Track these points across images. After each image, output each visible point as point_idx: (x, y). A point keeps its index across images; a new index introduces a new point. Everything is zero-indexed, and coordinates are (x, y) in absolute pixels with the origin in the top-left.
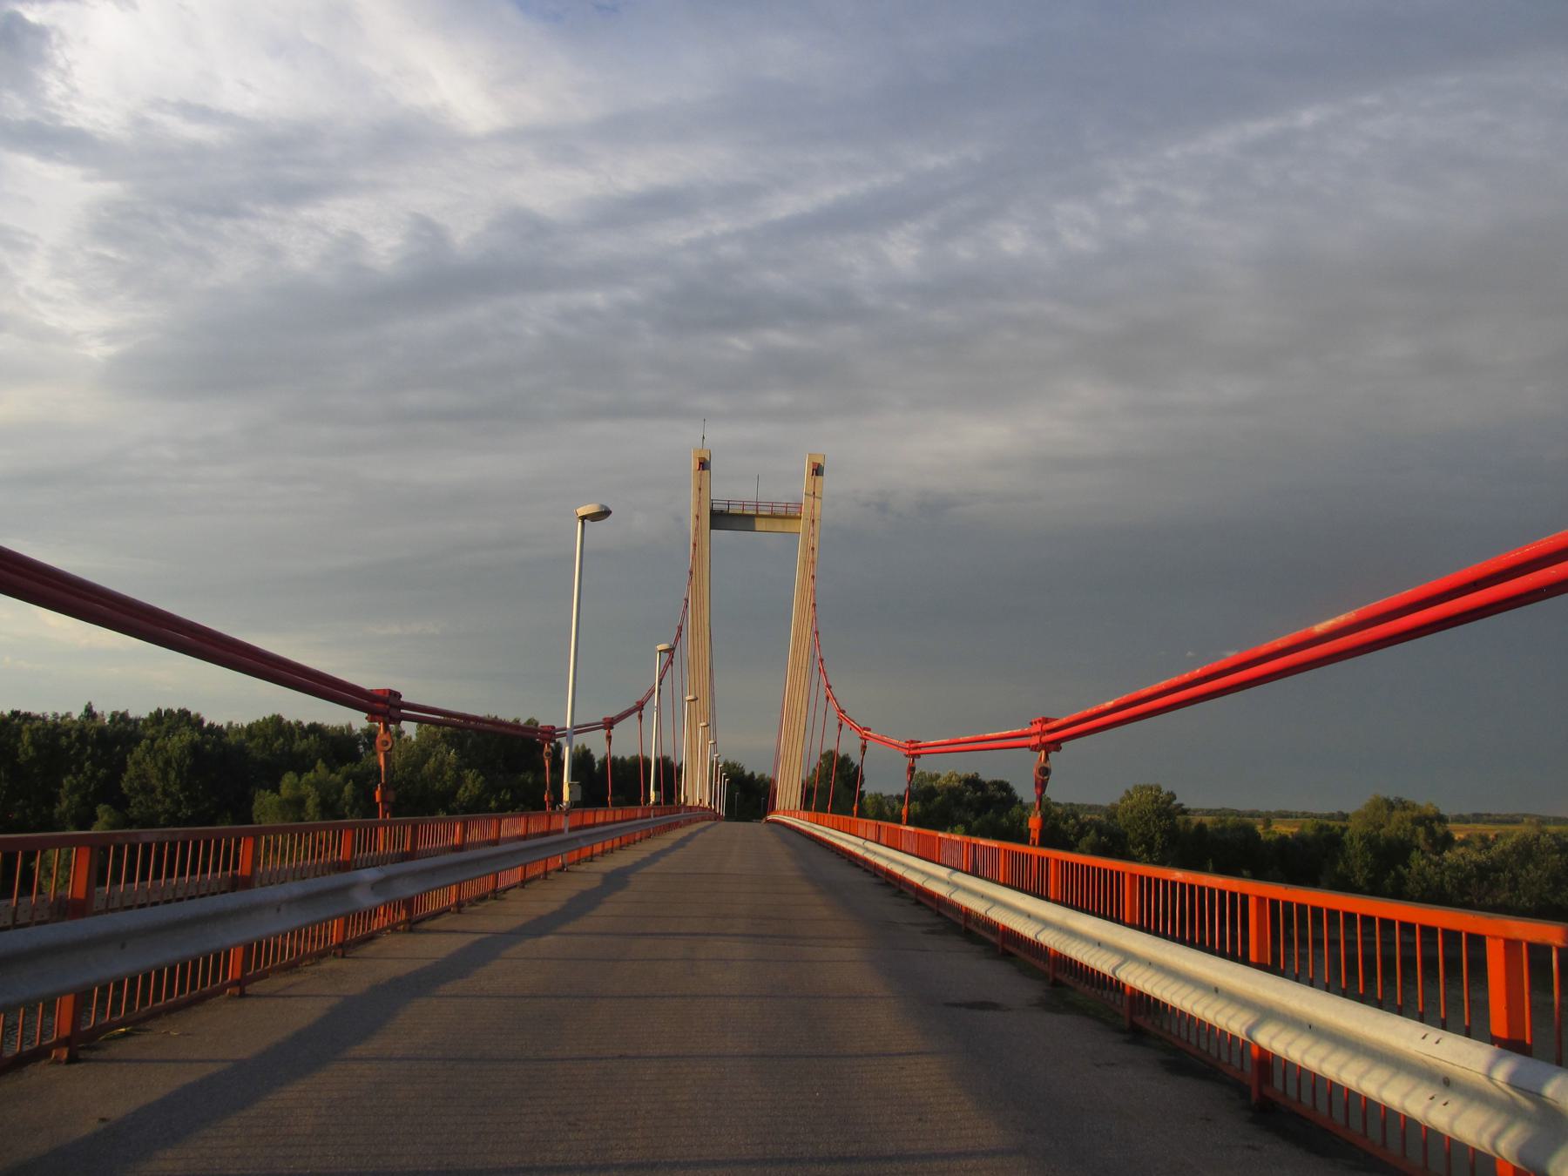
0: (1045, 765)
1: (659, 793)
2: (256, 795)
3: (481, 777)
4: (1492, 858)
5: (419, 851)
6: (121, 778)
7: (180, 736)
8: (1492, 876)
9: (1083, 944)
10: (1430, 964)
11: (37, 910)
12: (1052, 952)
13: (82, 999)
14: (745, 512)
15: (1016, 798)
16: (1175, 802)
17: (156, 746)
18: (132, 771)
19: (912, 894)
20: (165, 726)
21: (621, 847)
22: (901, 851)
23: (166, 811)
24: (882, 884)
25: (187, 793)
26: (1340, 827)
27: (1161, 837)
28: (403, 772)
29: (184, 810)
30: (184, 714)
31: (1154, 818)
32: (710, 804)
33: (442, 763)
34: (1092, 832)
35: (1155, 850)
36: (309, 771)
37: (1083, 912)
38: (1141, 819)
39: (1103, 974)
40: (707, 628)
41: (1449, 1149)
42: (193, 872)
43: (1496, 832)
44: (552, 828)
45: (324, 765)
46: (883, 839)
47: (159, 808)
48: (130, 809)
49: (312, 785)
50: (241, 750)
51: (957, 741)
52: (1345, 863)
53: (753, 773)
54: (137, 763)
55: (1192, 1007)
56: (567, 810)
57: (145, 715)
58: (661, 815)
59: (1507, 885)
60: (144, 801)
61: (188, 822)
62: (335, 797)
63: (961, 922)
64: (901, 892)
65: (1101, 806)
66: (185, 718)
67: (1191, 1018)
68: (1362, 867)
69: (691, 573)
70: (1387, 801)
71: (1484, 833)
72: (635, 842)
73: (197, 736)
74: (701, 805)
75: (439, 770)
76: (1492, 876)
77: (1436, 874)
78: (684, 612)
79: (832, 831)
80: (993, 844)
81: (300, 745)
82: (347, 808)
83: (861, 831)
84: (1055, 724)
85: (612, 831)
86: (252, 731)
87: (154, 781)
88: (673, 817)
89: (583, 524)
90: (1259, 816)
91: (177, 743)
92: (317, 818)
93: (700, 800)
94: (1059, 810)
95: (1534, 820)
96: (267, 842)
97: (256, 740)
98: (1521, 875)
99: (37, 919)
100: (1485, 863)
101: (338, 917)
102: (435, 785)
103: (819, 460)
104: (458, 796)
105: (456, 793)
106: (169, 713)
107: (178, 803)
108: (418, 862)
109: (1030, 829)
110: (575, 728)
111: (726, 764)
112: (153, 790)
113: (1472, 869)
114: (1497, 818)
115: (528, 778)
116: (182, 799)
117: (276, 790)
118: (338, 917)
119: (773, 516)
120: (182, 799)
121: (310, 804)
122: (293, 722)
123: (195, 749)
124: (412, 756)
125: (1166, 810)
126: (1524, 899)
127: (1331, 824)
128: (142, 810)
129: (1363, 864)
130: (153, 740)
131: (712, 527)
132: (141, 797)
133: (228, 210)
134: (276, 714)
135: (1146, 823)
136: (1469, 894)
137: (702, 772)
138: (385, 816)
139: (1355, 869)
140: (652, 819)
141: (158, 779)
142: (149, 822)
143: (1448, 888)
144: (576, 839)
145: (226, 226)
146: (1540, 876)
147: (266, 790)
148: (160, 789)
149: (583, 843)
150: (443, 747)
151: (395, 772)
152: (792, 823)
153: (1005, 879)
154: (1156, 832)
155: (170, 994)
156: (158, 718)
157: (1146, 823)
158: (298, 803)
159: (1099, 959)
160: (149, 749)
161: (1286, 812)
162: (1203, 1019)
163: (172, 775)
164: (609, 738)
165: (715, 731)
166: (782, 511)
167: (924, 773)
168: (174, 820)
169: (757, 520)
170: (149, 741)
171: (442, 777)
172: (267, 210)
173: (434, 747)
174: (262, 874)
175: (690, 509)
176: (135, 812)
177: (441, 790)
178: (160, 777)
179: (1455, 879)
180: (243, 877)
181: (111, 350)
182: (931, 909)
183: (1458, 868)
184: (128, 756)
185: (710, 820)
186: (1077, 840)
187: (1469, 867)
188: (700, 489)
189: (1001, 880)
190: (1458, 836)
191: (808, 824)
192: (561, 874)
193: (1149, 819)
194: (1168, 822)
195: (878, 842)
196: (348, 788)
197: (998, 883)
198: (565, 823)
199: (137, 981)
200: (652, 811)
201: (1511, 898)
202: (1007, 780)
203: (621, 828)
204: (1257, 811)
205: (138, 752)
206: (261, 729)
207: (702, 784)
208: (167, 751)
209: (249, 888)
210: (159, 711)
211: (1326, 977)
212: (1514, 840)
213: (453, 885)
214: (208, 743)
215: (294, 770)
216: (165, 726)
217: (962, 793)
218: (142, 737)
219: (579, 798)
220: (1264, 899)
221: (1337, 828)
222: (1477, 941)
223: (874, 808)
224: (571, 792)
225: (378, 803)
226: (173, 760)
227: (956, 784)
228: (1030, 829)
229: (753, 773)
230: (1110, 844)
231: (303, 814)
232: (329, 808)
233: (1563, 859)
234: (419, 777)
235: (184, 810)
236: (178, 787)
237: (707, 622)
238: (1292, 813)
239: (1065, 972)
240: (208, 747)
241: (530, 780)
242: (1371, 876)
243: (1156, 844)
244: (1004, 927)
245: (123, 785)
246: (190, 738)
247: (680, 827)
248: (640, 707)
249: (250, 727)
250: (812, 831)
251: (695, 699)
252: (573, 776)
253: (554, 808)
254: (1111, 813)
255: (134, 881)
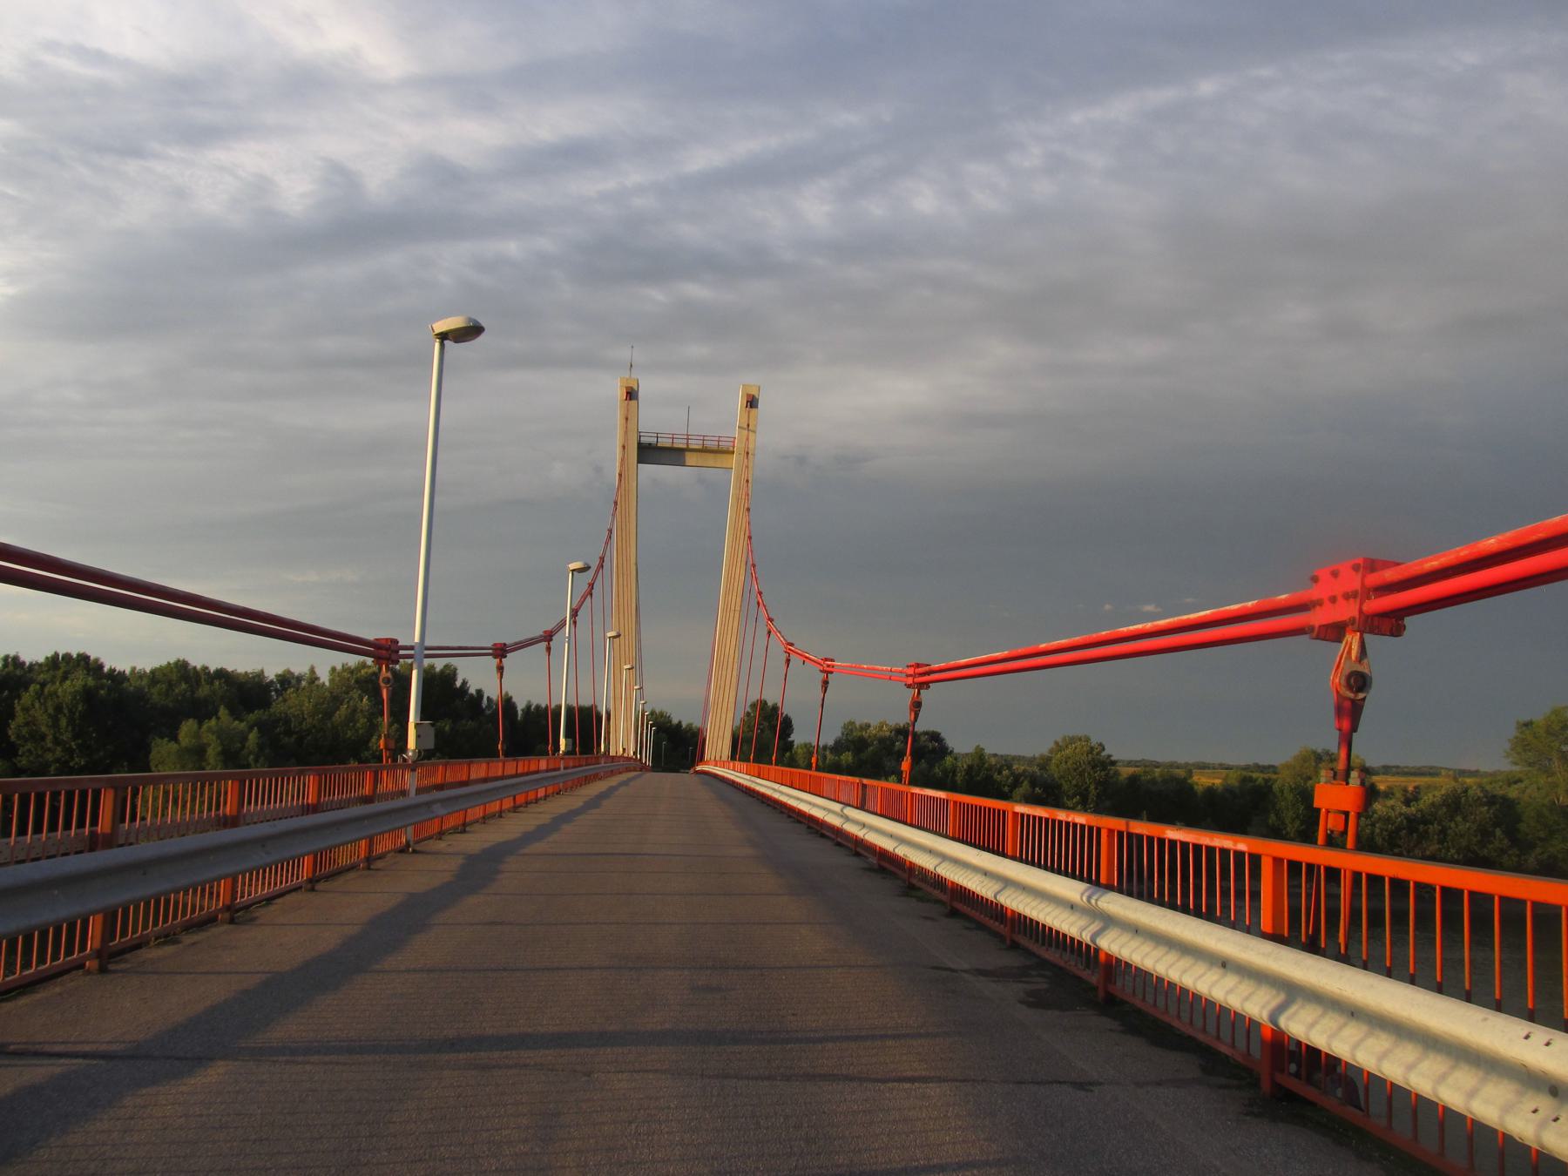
0: (1360, 668)
1: (570, 740)
2: (153, 744)
3: (396, 725)
4: (1421, 811)
5: (379, 795)
6: (9, 725)
7: (72, 680)
8: (1421, 827)
9: (994, 882)
10: (1400, 918)
11: (34, 848)
12: (1009, 914)
13: (110, 917)
14: (675, 446)
15: (947, 749)
16: (1103, 754)
17: (46, 690)
18: (20, 718)
19: (873, 860)
20: (61, 671)
21: (515, 809)
22: (823, 797)
23: (57, 760)
24: (871, 869)
25: (80, 741)
26: (1264, 779)
27: (1096, 788)
28: (313, 719)
29: (77, 759)
30: (84, 658)
31: (1089, 769)
32: (635, 753)
33: (355, 711)
34: (1026, 783)
35: (1090, 800)
36: (210, 718)
37: (1021, 862)
38: (1075, 770)
39: (1063, 934)
40: (633, 568)
41: (1472, 1133)
42: (38, 829)
43: (1416, 784)
44: (519, 772)
45: (227, 712)
46: (870, 804)
47: (49, 757)
48: (19, 758)
49: (213, 733)
50: (140, 697)
51: (1034, 651)
52: (1276, 815)
53: (680, 722)
54: (26, 710)
55: (1434, 1090)
56: (414, 762)
57: (41, 660)
58: (574, 767)
59: (1436, 837)
60: (32, 749)
61: (81, 771)
62: (239, 745)
63: (1094, 978)
64: (912, 887)
65: (1024, 757)
66: (84, 662)
67: (1197, 997)
68: (1293, 820)
69: (616, 503)
70: (1314, 752)
71: (1403, 784)
72: (537, 801)
73: (91, 682)
74: (626, 755)
75: (352, 718)
76: (1421, 827)
77: (1367, 825)
78: (607, 543)
79: (759, 781)
80: (941, 794)
81: (204, 691)
82: (252, 757)
83: (827, 788)
84: (1389, 575)
85: (497, 789)
86: (155, 677)
87: (44, 729)
88: (591, 769)
89: (573, 574)
90: (1178, 768)
91: (67, 689)
92: (219, 767)
93: (624, 750)
94: (993, 761)
95: (1451, 773)
96: (166, 793)
97: (158, 686)
98: (1451, 828)
99: (33, 856)
100: (1414, 815)
101: (225, 877)
102: (347, 734)
103: (754, 392)
104: (370, 745)
105: (369, 740)
106: (67, 657)
107: (70, 752)
108: (116, 851)
109: (1318, 810)
110: (428, 649)
111: (652, 713)
112: (43, 737)
113: (1402, 821)
114: (1406, 770)
115: (445, 726)
116: (74, 747)
117: (174, 738)
118: (308, 854)
119: (704, 450)
120: (74, 747)
121: (211, 753)
122: (199, 667)
123: (88, 695)
124: (323, 703)
125: (1101, 764)
126: (1453, 851)
127: (1254, 775)
128: (31, 759)
129: (1294, 816)
130: (43, 685)
131: (640, 461)
132: (29, 746)
133: (134, 151)
134: (181, 659)
135: (1081, 774)
136: (1400, 847)
137: (626, 720)
138: (387, 761)
139: (1287, 821)
140: (562, 771)
141: (47, 726)
142: (42, 770)
143: (1379, 840)
144: (428, 804)
145: (132, 167)
146: (1468, 829)
147: (162, 738)
148: (51, 737)
149: (440, 810)
150: (355, 694)
151: (304, 719)
152: (726, 775)
153: (954, 832)
154: (1090, 783)
155: (41, 960)
156: (54, 662)
157: (1081, 774)
158: (199, 753)
159: (990, 888)
160: (39, 695)
161: (1203, 763)
162: (1119, 957)
163: (63, 722)
164: (500, 669)
165: (641, 675)
166: (710, 444)
167: (854, 723)
168: (65, 768)
169: (688, 455)
170: (38, 686)
171: (354, 726)
172: (174, 152)
173: (347, 693)
174: (149, 827)
175: (612, 451)
176: (23, 762)
177: (353, 738)
178: (50, 724)
179: (1386, 831)
180: (104, 835)
181: (11, 291)
182: (996, 935)
183: (1388, 820)
184: (16, 701)
185: (635, 770)
186: (1011, 791)
187: (1399, 819)
188: (627, 419)
189: (879, 812)
190: (1382, 787)
191: (748, 777)
192: (405, 856)
193: (1084, 770)
194: (1103, 773)
195: (862, 807)
196: (253, 736)
197: (946, 836)
198: (411, 781)
199: (76, 925)
200: (562, 762)
201: (1440, 850)
202: (938, 730)
203: (513, 786)
204: (1176, 762)
205: (27, 697)
206: (164, 675)
207: (627, 731)
208: (58, 697)
209: (236, 827)
210: (56, 654)
211: (1497, 992)
212: (1443, 792)
213: (362, 839)
214: (103, 689)
215: (195, 718)
216: (61, 671)
217: (893, 744)
218: (32, 681)
219: (430, 744)
220: (1282, 860)
221: (1260, 780)
222: (1256, 860)
223: (805, 758)
224: (418, 736)
225: (382, 750)
226: (64, 706)
227: (888, 734)
228: (1318, 810)
229: (680, 722)
230: (1044, 796)
231: (204, 764)
232: (231, 757)
233: (1491, 811)
234: (329, 725)
235: (77, 759)
236: (69, 735)
237: (633, 561)
238: (1209, 764)
239: (1050, 945)
240: (102, 692)
241: (447, 728)
242: (1303, 827)
243: (1091, 796)
244: (953, 883)
245: (10, 732)
246: (83, 683)
247: (600, 779)
248: (548, 637)
249: (153, 672)
250: (753, 786)
251: (632, 668)
252: (425, 713)
253: (554, 754)
254: (1044, 763)
255: (27, 834)
